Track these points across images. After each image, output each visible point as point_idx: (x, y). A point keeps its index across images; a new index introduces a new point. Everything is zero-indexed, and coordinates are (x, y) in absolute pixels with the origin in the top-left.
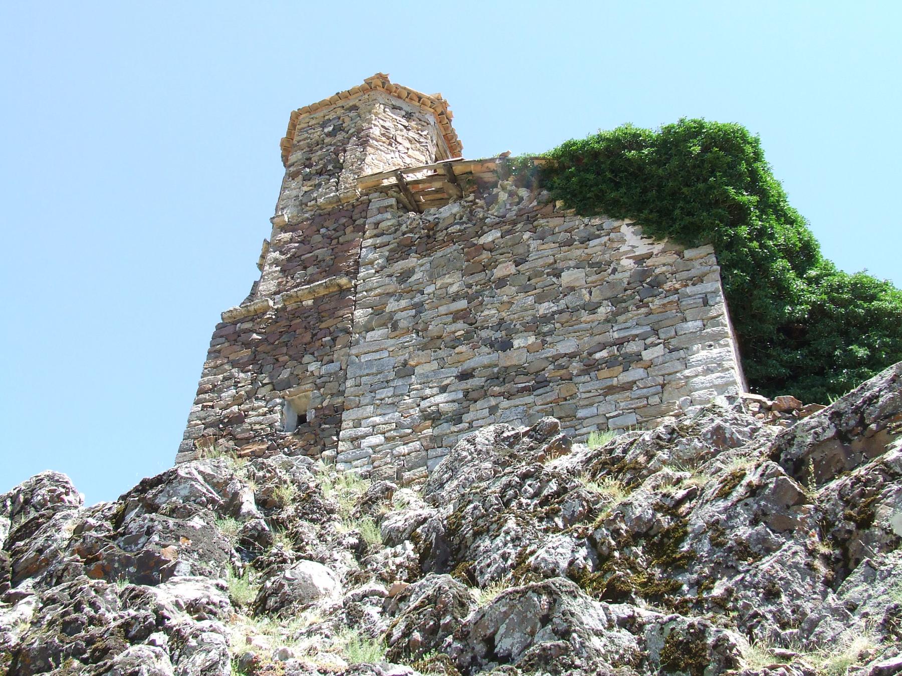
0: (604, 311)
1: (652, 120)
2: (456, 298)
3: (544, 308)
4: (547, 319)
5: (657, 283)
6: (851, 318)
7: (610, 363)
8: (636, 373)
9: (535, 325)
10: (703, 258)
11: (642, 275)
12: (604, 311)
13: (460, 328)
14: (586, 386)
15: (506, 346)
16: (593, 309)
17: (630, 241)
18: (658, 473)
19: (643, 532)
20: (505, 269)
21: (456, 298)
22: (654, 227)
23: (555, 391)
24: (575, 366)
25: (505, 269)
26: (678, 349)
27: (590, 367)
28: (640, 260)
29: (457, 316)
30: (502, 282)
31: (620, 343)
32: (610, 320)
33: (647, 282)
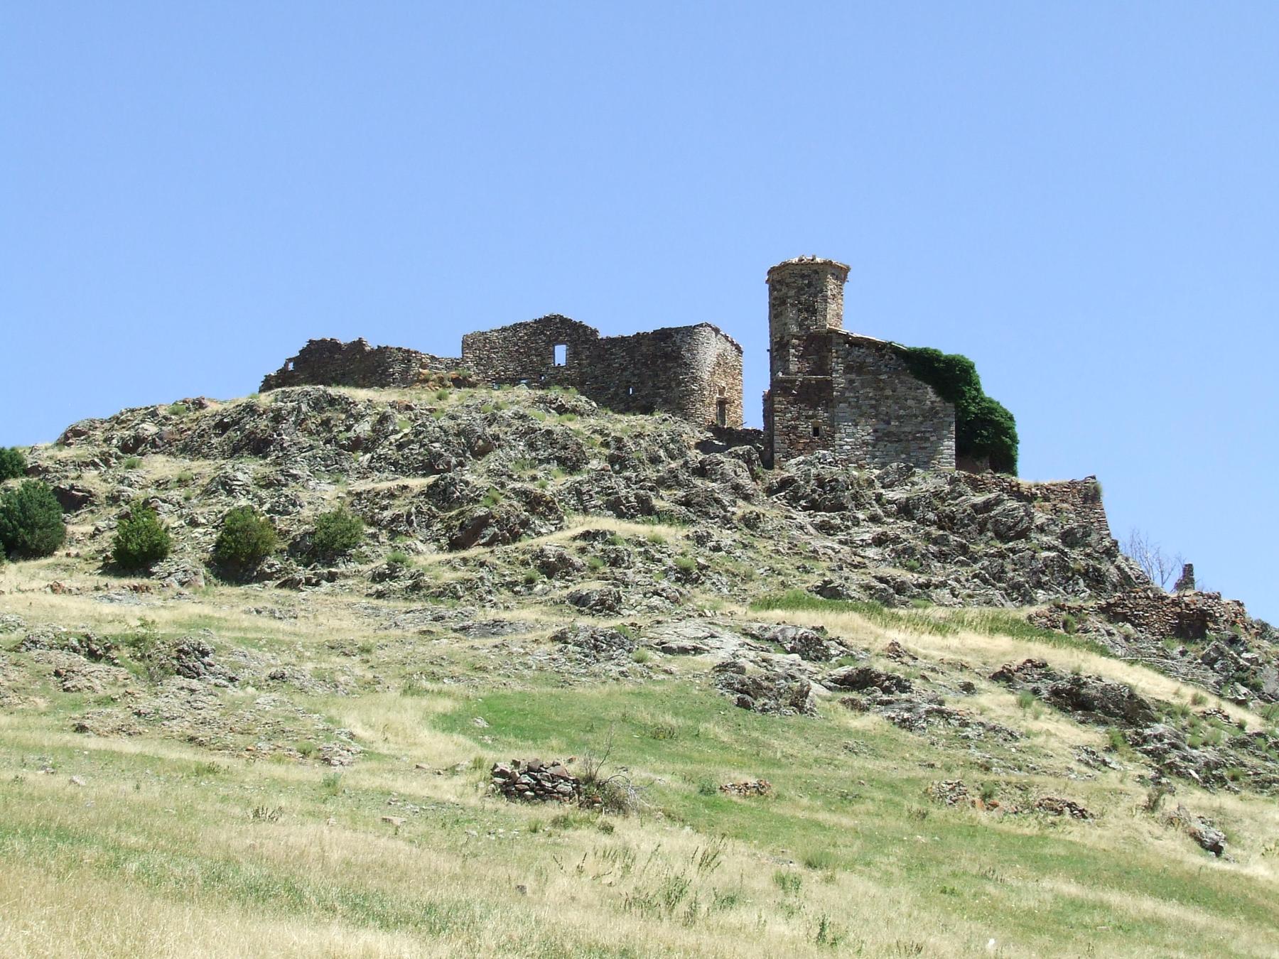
0: (920, 419)
1: (947, 350)
2: (871, 398)
3: (901, 412)
4: (902, 417)
5: (937, 413)
6: (985, 420)
7: (921, 438)
8: (928, 445)
9: (898, 418)
10: (950, 406)
11: (933, 408)
12: (920, 419)
13: (873, 412)
14: (913, 445)
15: (888, 423)
16: (916, 417)
17: (930, 395)
18: (842, 671)
19: (947, 516)
20: (888, 392)
21: (871, 398)
22: (938, 392)
23: (904, 444)
24: (910, 437)
25: (888, 392)
26: (940, 439)
27: (915, 439)
28: (932, 402)
29: (872, 406)
30: (887, 398)
31: (924, 432)
32: (921, 423)
33: (933, 412)
